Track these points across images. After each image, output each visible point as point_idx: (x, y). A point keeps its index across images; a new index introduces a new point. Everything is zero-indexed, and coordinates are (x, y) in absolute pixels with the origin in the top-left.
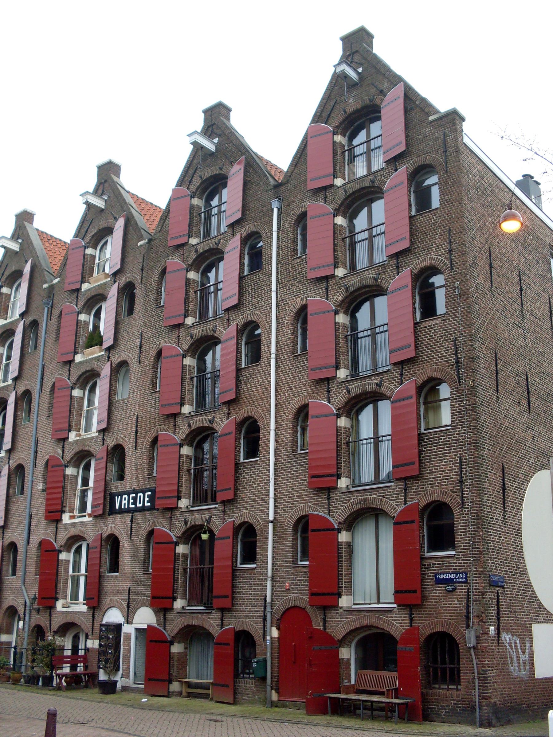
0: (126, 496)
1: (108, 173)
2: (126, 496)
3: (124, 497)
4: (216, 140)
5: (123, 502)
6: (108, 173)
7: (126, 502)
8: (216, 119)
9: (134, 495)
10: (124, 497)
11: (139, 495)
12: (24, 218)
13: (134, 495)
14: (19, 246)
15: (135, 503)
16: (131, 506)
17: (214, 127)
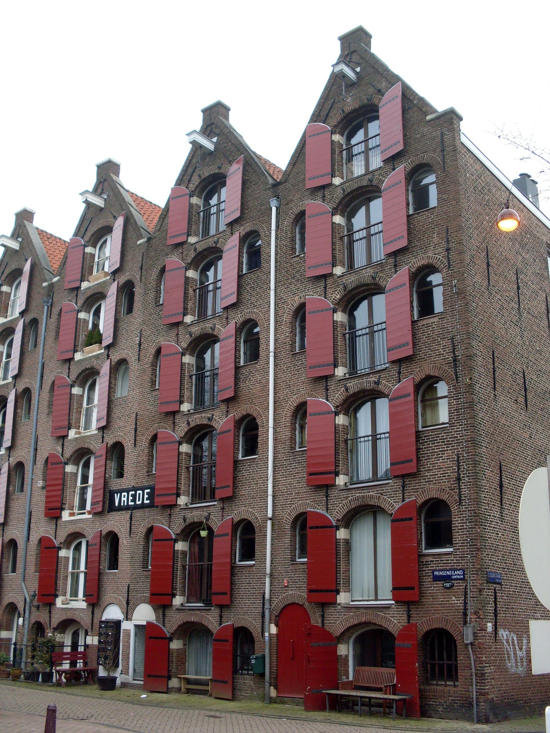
0: (126, 494)
1: (107, 172)
2: (126, 494)
3: (123, 494)
4: (215, 140)
5: (123, 499)
6: (107, 172)
7: (125, 499)
8: (215, 118)
9: (133, 492)
10: (123, 494)
11: (138, 492)
12: (24, 217)
13: (133, 492)
14: (18, 245)
15: (134, 500)
16: (130, 503)
17: (213, 126)
